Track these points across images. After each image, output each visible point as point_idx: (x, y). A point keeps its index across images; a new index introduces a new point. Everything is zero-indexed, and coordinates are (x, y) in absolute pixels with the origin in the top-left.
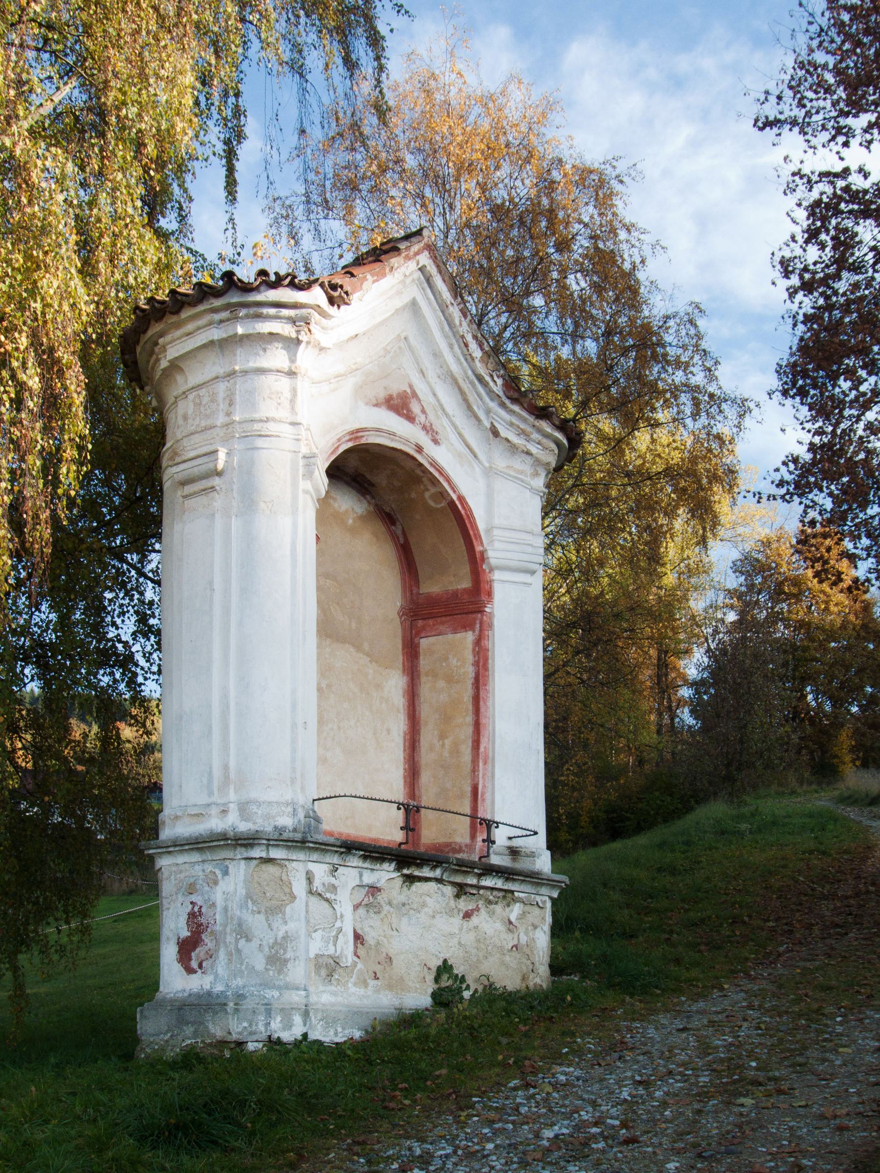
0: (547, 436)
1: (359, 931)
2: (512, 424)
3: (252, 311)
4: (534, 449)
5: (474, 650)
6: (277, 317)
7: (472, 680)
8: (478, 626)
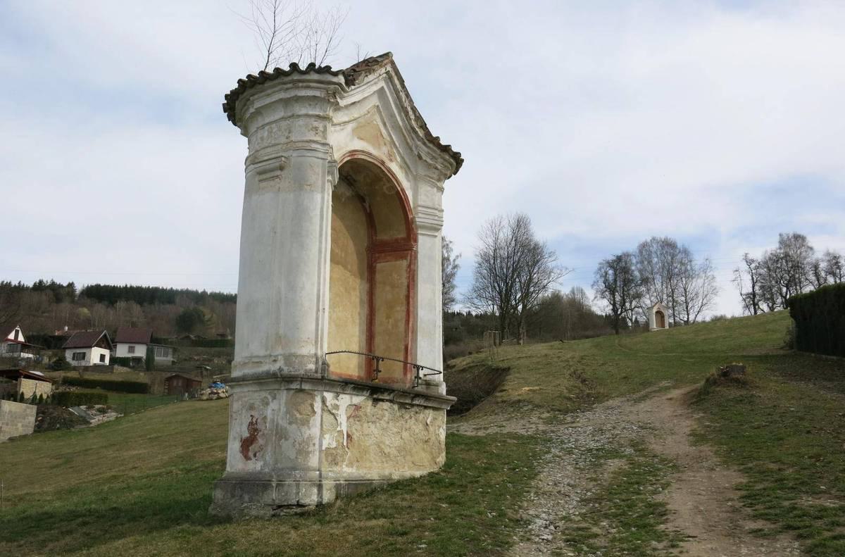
3: (305, 84)
4: (439, 167)
5: (406, 270)
7: (406, 287)
8: (409, 258)
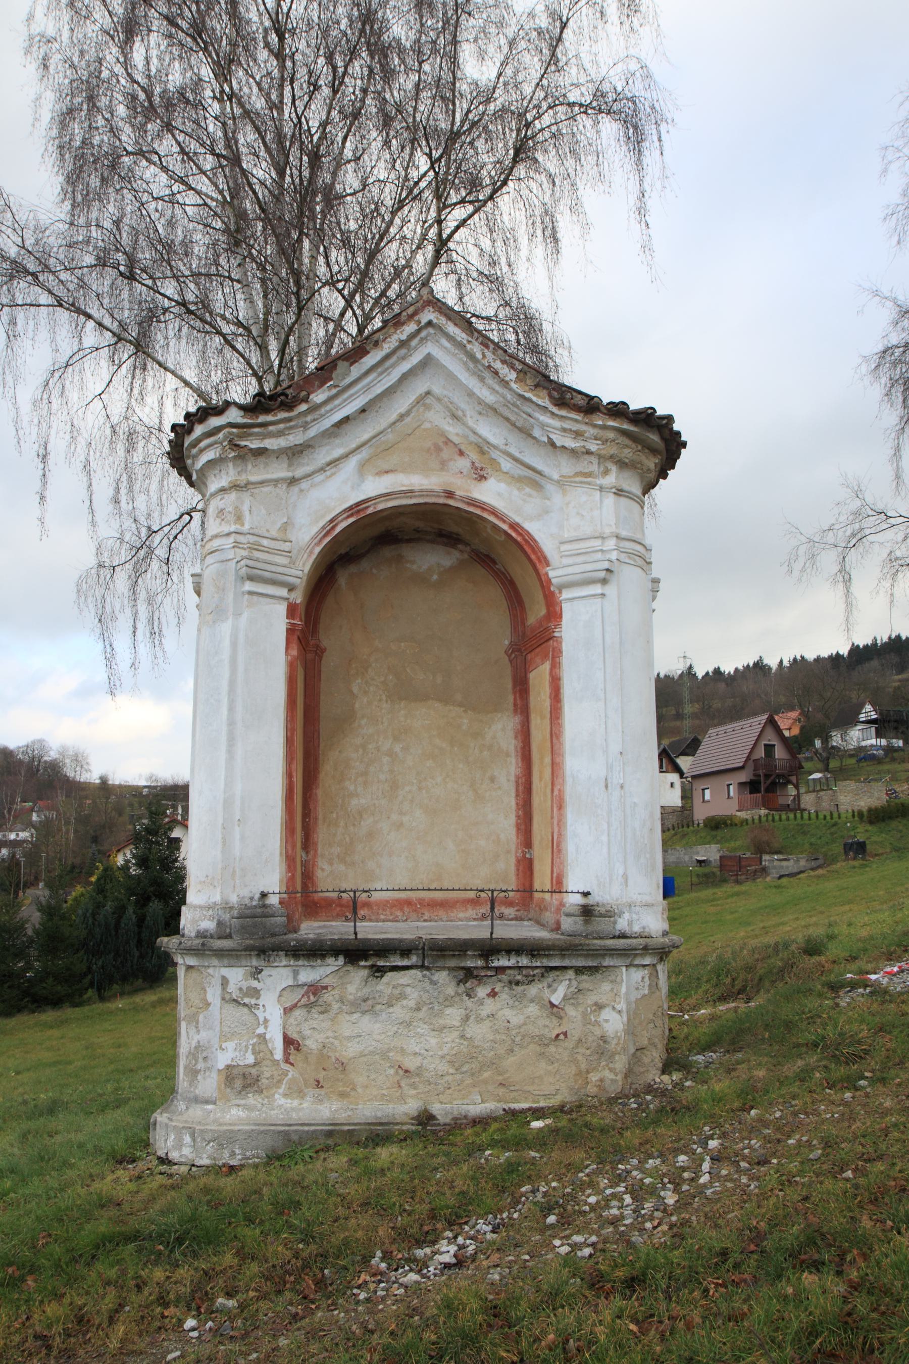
0: (604, 427)
1: (295, 1036)
2: (564, 430)
4: (593, 447)
6: (201, 451)
